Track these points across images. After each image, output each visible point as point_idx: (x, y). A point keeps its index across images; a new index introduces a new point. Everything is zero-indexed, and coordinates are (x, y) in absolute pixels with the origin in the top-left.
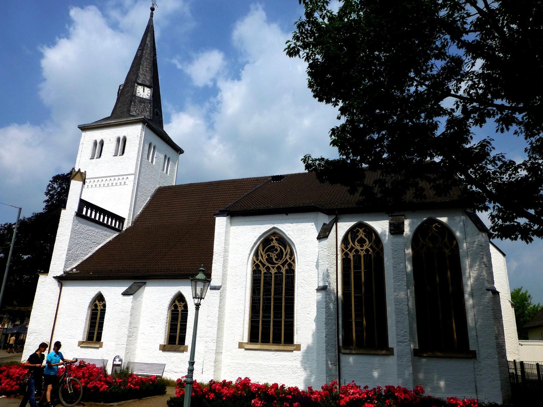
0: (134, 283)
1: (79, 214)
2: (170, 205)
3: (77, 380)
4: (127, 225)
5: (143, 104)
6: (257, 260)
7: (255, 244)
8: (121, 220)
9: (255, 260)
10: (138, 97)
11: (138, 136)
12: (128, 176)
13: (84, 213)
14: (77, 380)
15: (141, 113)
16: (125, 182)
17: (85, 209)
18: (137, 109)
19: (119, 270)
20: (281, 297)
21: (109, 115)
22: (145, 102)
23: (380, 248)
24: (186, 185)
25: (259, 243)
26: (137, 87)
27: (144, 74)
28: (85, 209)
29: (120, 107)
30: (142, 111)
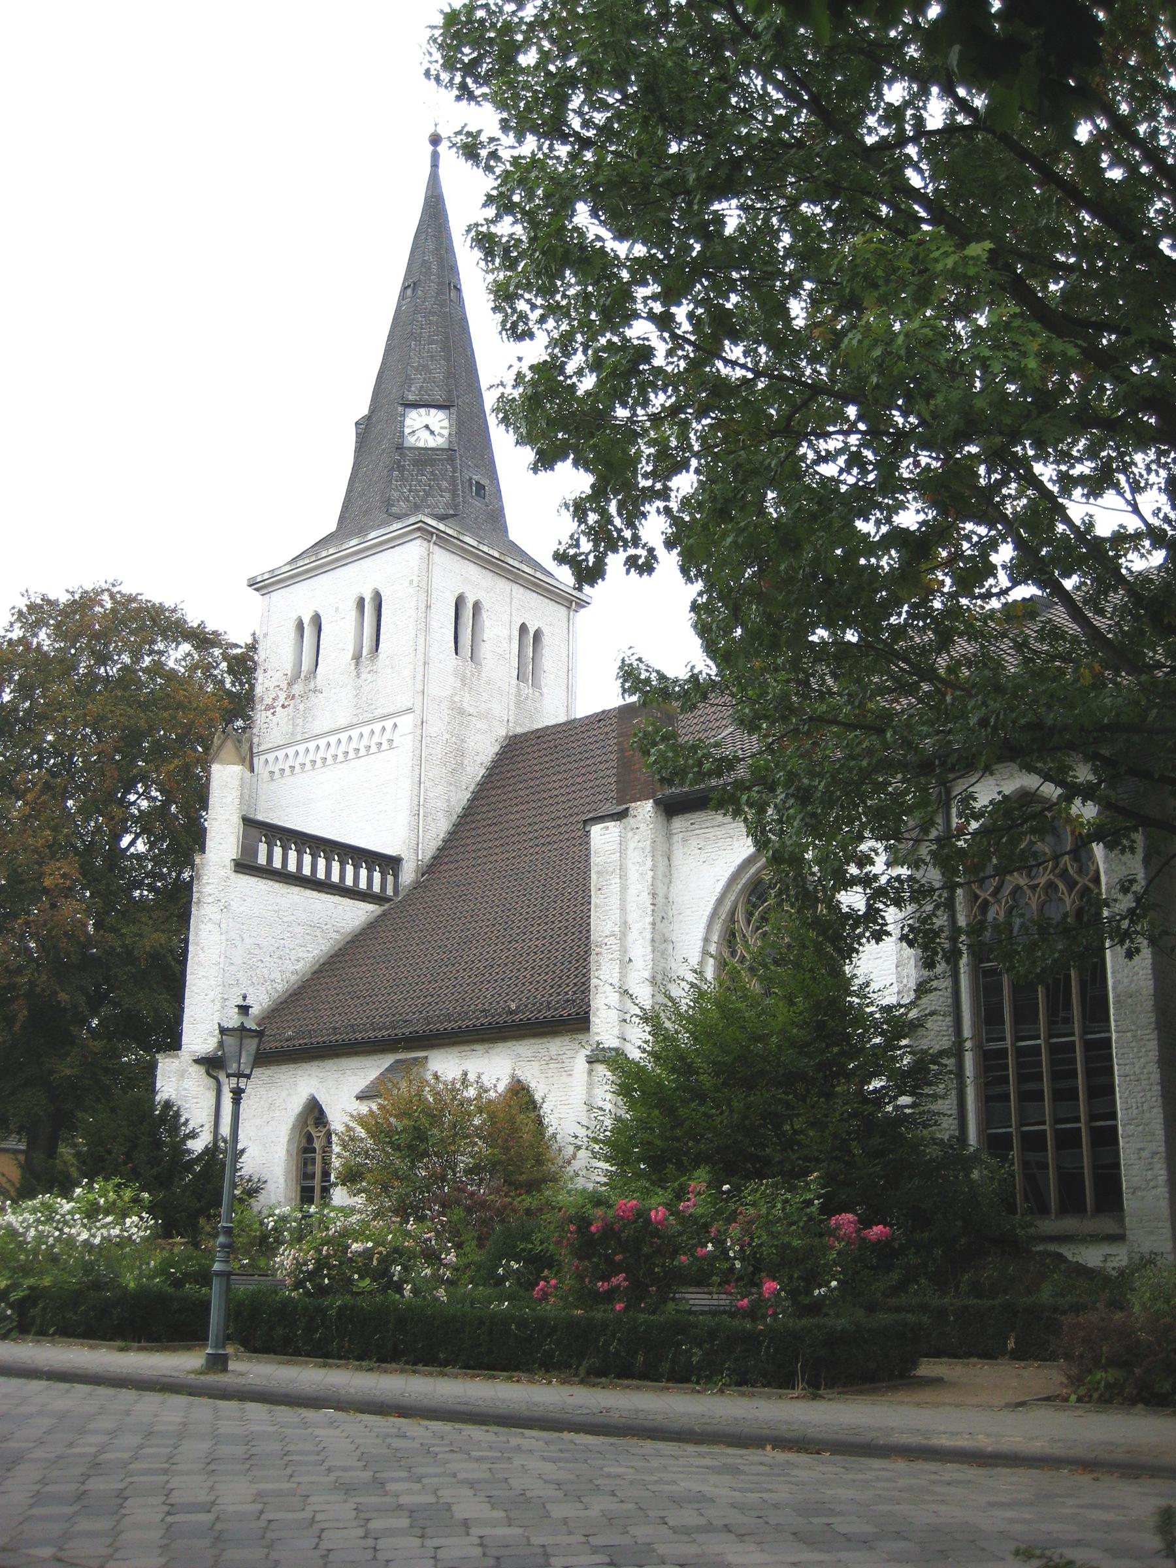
0: (397, 1061)
1: (245, 866)
2: (537, 796)
3: (988, 1303)
4: (408, 875)
5: (429, 469)
6: (733, 954)
7: (720, 901)
8: (390, 864)
9: (726, 955)
10: (410, 449)
11: (411, 582)
12: (396, 720)
13: (262, 860)
14: (988, 1303)
15: (424, 500)
16: (390, 741)
17: (263, 848)
18: (410, 491)
19: (335, 1028)
20: (1106, 1035)
21: (332, 527)
22: (435, 460)
23: (1092, 873)
24: (587, 717)
25: (732, 897)
26: (403, 415)
27: (423, 366)
28: (263, 848)
29: (361, 495)
30: (427, 494)
